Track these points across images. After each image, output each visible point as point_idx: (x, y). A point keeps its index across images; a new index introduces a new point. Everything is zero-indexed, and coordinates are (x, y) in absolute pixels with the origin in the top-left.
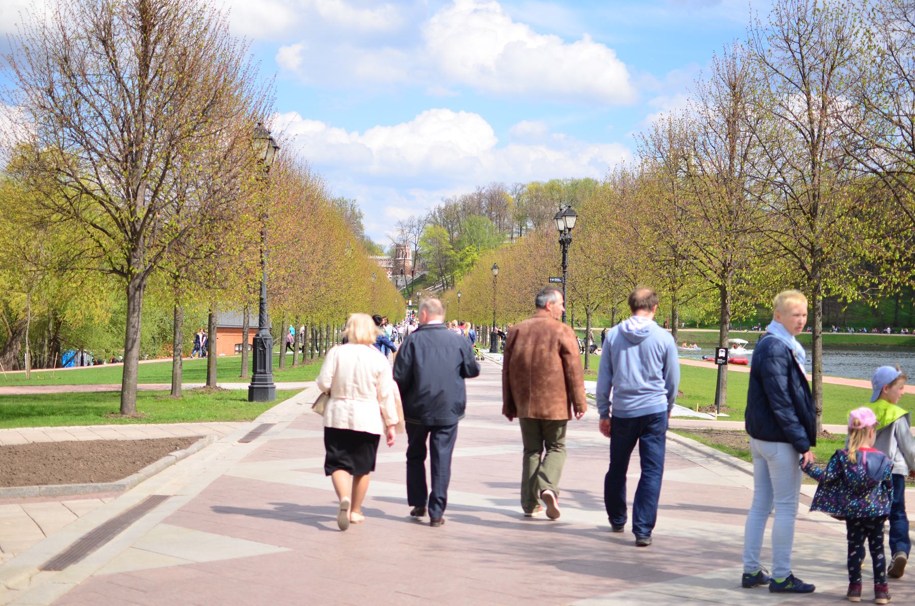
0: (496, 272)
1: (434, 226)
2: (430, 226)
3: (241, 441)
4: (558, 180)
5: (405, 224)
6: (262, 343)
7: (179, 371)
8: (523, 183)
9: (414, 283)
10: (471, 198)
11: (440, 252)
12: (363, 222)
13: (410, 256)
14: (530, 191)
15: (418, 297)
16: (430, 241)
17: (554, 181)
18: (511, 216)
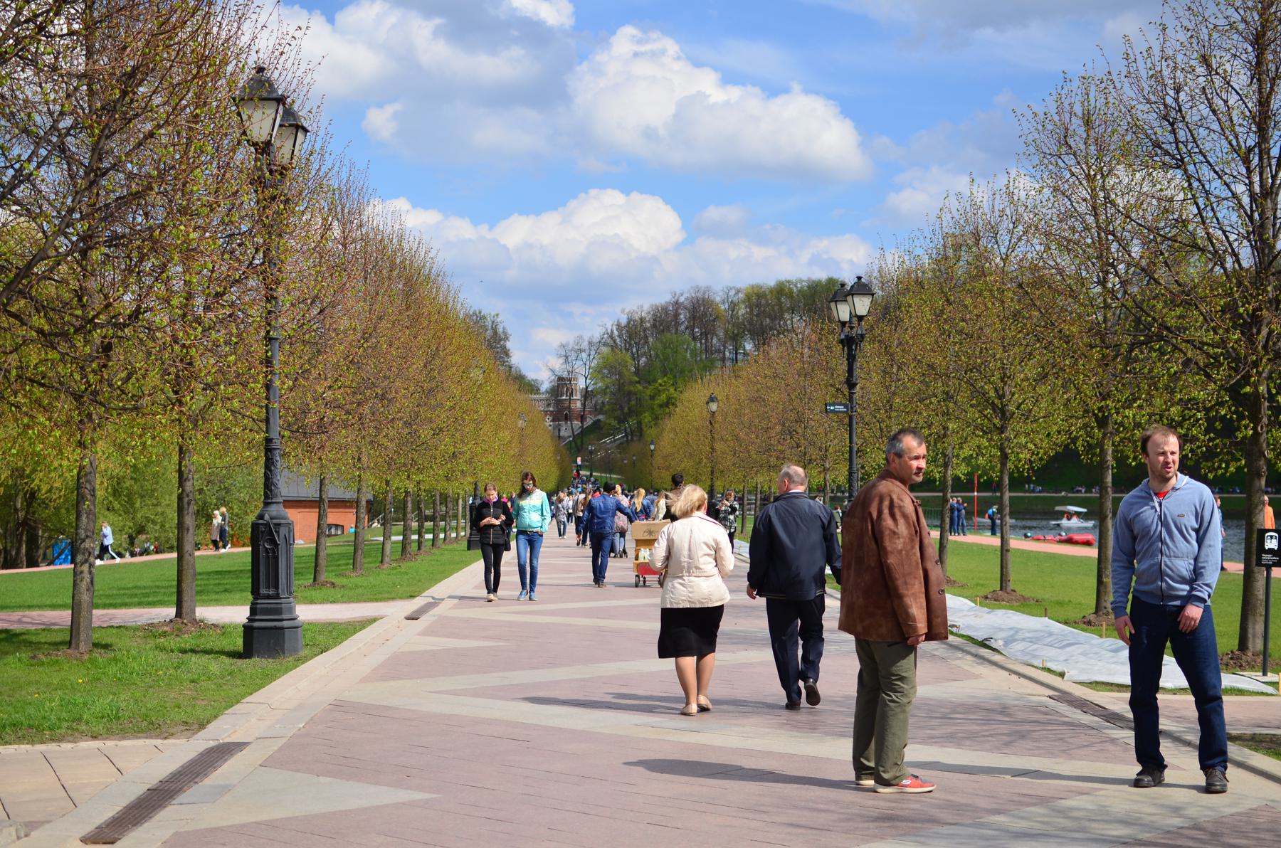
0: (714, 406)
1: (612, 349)
2: (605, 350)
3: (85, 840)
4: (788, 282)
5: (570, 347)
6: (271, 533)
7: (85, 597)
8: (739, 286)
9: (584, 432)
10: (665, 309)
11: (620, 387)
12: (509, 345)
13: (578, 393)
14: (748, 298)
15: (591, 452)
16: (605, 371)
17: (782, 283)
18: (721, 334)
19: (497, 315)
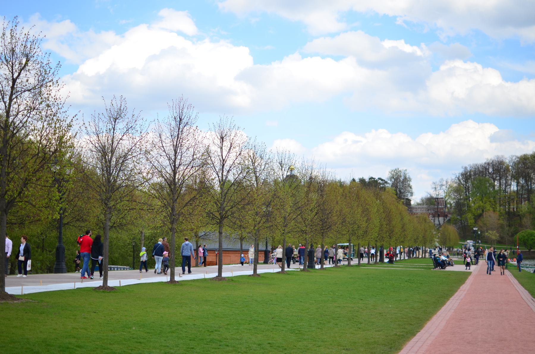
12: (411, 184)
19: (406, 170)
